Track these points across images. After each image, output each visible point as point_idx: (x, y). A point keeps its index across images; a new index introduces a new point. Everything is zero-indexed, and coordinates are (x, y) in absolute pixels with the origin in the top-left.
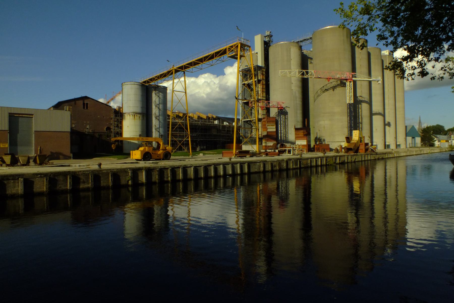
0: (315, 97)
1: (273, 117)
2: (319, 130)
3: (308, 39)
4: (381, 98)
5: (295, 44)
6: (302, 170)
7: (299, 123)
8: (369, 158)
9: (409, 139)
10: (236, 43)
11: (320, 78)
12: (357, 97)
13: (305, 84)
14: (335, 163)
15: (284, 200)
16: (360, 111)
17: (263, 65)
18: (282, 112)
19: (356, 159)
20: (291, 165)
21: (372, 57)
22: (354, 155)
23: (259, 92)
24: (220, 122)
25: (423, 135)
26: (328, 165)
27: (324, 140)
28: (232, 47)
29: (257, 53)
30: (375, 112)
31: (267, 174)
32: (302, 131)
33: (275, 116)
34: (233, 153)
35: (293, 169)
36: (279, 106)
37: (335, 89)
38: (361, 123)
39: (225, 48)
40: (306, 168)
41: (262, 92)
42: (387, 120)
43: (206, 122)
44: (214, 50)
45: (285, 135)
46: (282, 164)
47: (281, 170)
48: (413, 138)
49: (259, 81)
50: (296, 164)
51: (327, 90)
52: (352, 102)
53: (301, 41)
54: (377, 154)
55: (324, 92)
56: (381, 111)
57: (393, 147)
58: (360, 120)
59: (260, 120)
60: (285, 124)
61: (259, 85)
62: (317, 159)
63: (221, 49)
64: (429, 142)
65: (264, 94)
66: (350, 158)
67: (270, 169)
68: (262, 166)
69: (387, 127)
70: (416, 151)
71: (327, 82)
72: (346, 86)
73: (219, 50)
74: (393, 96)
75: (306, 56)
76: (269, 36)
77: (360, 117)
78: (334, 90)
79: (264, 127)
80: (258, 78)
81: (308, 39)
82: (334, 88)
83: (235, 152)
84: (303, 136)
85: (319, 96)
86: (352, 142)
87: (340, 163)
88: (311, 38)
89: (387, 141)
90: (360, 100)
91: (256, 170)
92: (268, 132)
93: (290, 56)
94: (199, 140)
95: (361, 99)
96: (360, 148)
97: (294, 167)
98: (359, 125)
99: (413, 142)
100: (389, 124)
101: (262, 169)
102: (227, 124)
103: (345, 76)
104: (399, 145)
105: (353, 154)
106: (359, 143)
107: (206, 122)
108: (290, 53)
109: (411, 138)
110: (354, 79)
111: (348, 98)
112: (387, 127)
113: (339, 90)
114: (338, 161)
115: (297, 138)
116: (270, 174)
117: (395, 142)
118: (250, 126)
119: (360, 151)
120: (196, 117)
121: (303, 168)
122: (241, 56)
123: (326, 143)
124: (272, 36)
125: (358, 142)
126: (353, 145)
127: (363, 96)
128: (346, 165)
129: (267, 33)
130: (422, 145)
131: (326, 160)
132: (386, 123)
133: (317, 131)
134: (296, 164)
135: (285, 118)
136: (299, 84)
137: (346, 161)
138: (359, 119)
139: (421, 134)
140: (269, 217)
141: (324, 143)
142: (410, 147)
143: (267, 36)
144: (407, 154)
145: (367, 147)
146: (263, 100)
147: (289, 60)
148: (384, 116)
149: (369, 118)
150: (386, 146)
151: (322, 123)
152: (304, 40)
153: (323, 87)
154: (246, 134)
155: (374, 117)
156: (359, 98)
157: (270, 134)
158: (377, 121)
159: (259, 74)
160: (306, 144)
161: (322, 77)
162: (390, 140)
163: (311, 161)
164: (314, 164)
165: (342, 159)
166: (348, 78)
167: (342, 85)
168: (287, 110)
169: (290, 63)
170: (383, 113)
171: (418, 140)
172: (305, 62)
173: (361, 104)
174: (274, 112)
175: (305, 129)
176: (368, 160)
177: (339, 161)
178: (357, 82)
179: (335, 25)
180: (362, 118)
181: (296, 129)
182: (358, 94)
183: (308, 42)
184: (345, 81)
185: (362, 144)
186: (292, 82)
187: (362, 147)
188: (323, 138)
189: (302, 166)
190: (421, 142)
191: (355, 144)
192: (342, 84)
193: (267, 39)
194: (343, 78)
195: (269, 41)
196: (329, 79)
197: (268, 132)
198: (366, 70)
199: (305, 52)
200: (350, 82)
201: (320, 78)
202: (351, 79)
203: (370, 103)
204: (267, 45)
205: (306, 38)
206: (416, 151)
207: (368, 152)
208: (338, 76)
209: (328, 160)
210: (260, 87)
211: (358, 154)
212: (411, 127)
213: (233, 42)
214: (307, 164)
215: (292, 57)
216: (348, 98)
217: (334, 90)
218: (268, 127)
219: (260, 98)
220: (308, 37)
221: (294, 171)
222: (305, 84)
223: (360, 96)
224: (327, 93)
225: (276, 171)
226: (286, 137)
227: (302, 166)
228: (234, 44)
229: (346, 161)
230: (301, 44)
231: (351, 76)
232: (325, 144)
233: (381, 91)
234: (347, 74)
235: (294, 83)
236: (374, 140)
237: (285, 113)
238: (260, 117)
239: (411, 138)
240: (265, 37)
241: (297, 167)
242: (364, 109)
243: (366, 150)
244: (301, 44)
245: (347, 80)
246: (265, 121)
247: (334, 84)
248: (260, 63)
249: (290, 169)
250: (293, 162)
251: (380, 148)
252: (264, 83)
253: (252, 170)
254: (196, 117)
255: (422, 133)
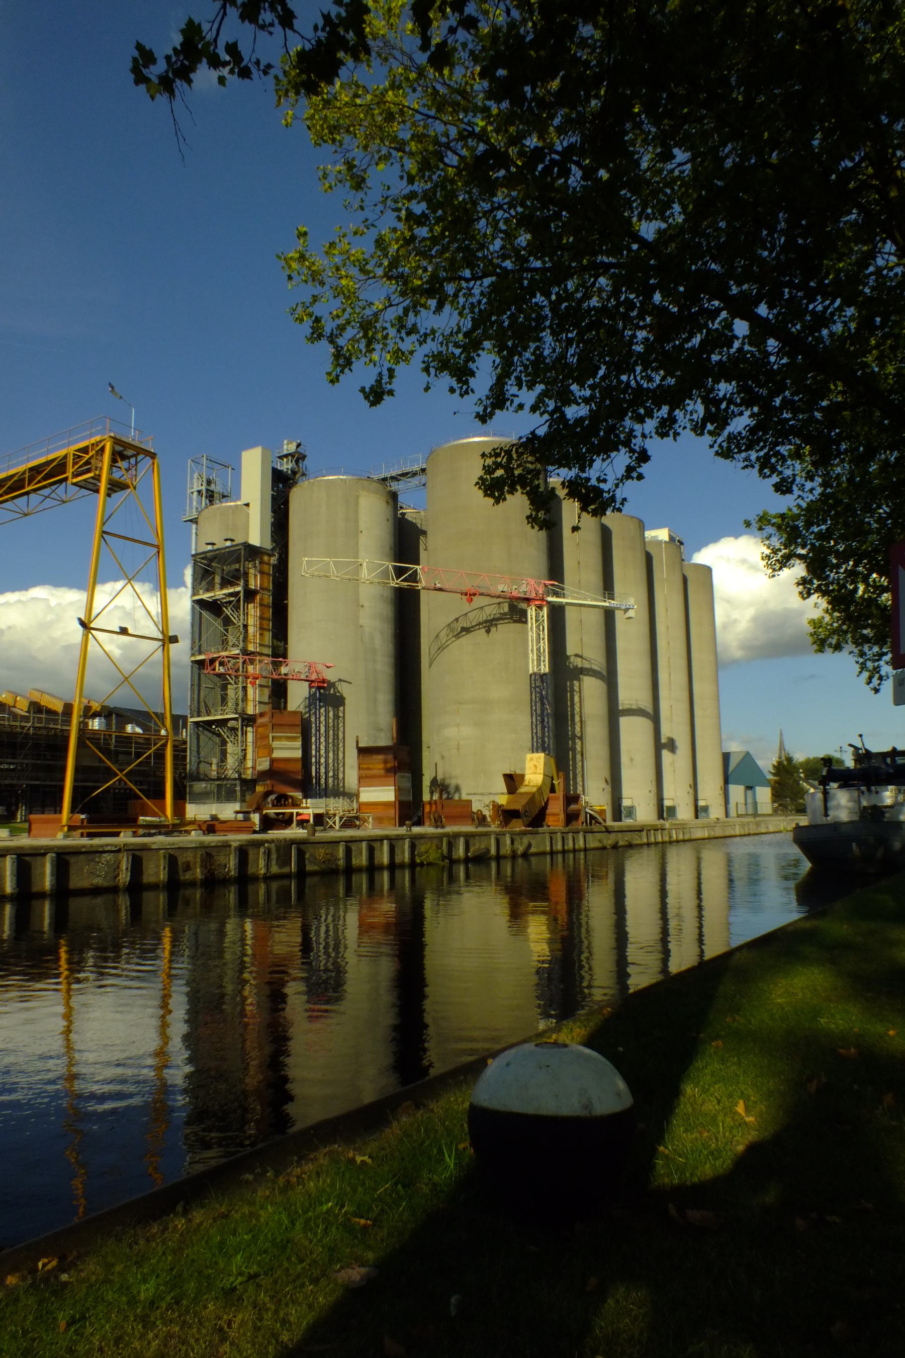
0: (432, 653)
1: (295, 713)
2: (443, 757)
3: (414, 474)
4: (643, 665)
5: (375, 485)
6: (309, 881)
7: (382, 735)
8: (581, 844)
9: (737, 792)
10: (98, 438)
11: (440, 590)
12: (568, 658)
13: (405, 609)
14: (449, 856)
15: (327, 988)
16: (576, 699)
17: (268, 545)
18: (326, 695)
19: (529, 846)
20: (262, 863)
21: (689, 583)
22: (524, 833)
23: (251, 630)
24: (109, 725)
25: (776, 782)
26: (422, 864)
27: (457, 789)
28: (85, 450)
29: (247, 505)
30: (626, 707)
31: (148, 897)
32: (381, 757)
33: (302, 709)
34: (60, 820)
35: (269, 878)
36: (314, 677)
37: (493, 629)
38: (581, 738)
39: (62, 453)
40: (329, 873)
41: (261, 628)
42: (666, 732)
43: (55, 722)
44: (28, 460)
45: (336, 771)
46: (221, 859)
47: (213, 882)
48: (749, 788)
49: (250, 595)
50: (284, 860)
51: (466, 630)
52: (545, 668)
53: (393, 478)
54: (609, 832)
55: (458, 636)
56: (645, 703)
57: (684, 813)
58: (578, 729)
59: (249, 720)
60: (336, 736)
61: (251, 606)
62: (376, 845)
63: (51, 457)
64: (794, 800)
65: (268, 636)
66: (508, 842)
67: (163, 876)
68: (125, 863)
69: (665, 753)
70: (743, 825)
71: (466, 607)
72: (526, 622)
73: (42, 460)
74: (683, 663)
75: (412, 525)
76: (292, 455)
77: (577, 718)
78: (488, 631)
79: (263, 745)
80: (249, 585)
81: (414, 474)
82: (489, 625)
83: (70, 819)
84: (382, 772)
85: (441, 648)
86: (522, 790)
87: (467, 860)
88: (423, 470)
89: (666, 795)
90: (576, 667)
91: (98, 881)
92: (273, 761)
93: (356, 521)
94: (24, 783)
95: (578, 663)
96: (548, 811)
97: (275, 869)
98: (574, 743)
99: (750, 800)
100: (671, 746)
101: (124, 877)
102: (139, 730)
103: (524, 588)
104: (706, 809)
105: (523, 828)
106: (547, 794)
107: (55, 722)
108: (356, 512)
109: (741, 788)
110: (550, 599)
111: (532, 656)
112: (666, 754)
113: (505, 631)
114: (460, 852)
115: (365, 779)
116: (162, 898)
117: (690, 800)
118: (217, 740)
119: (550, 820)
120: (22, 707)
121: (314, 873)
122: (115, 486)
123: (465, 797)
124: (304, 457)
125: (540, 789)
126: (524, 801)
127: (584, 655)
128: (493, 865)
129: (289, 447)
130: (775, 811)
131: (413, 847)
132: (663, 740)
133: (437, 758)
134: (284, 860)
135: (336, 717)
136: (387, 610)
137: (493, 851)
138: (573, 724)
139: (770, 777)
140: (278, 1037)
141: (456, 797)
142: (738, 816)
143: (286, 456)
144: (712, 834)
145: (573, 807)
146: (261, 654)
147: (354, 532)
148: (655, 718)
149: (605, 723)
150: (663, 811)
151: (451, 732)
152: (404, 475)
153: (457, 620)
154: (203, 766)
155: (624, 721)
156: (572, 659)
157: (282, 766)
158: (634, 735)
159: (252, 571)
160: (393, 799)
161: (446, 586)
162: (676, 793)
163: (348, 852)
164: (384, 858)
165: (477, 847)
166: (533, 595)
167: (516, 617)
168: (344, 689)
169: (357, 543)
170: (650, 709)
171: (764, 794)
172: (406, 542)
173: (579, 680)
174: (298, 696)
175: (404, 751)
176: (574, 851)
177: (467, 849)
178: (567, 608)
179: (495, 435)
180: (581, 721)
181: (363, 751)
182: (571, 648)
183: (415, 481)
184: (523, 605)
185: (557, 799)
186: (361, 602)
187: (556, 808)
188: (453, 782)
189: (309, 868)
190: (774, 801)
191: (532, 798)
192: (516, 612)
193: (286, 466)
194: (515, 594)
195: (294, 473)
196: (470, 596)
197: (273, 761)
198: (593, 576)
199: (410, 513)
200: (540, 607)
201: (440, 590)
202: (543, 600)
203: (610, 678)
204: (282, 484)
205: (408, 470)
206: (743, 825)
207: (578, 825)
208: (501, 588)
209: (422, 848)
210: (253, 612)
211: (540, 830)
212: (742, 755)
213: (91, 436)
214: (334, 858)
215: (362, 525)
216: (532, 656)
217: (488, 631)
218: (275, 744)
219: (251, 648)
220: (416, 468)
221: (275, 885)
222: (405, 609)
223: (577, 655)
224: (465, 640)
225: (192, 884)
226: (336, 777)
227: (309, 868)
228: (93, 441)
229: (493, 851)
230: (395, 486)
231: (541, 591)
232: (460, 800)
233: (645, 646)
234: (529, 581)
235: (366, 604)
236: (626, 791)
237: (338, 701)
238: (250, 711)
239: (741, 788)
240: (281, 458)
241: (286, 870)
242: (590, 696)
243: (571, 818)
244: (395, 486)
245: (528, 600)
246: (263, 725)
247: (491, 611)
248: (256, 534)
249: (255, 879)
250: (268, 853)
251: (644, 813)
252: (268, 599)
253: (77, 881)
254: (22, 707)
255: (774, 774)
